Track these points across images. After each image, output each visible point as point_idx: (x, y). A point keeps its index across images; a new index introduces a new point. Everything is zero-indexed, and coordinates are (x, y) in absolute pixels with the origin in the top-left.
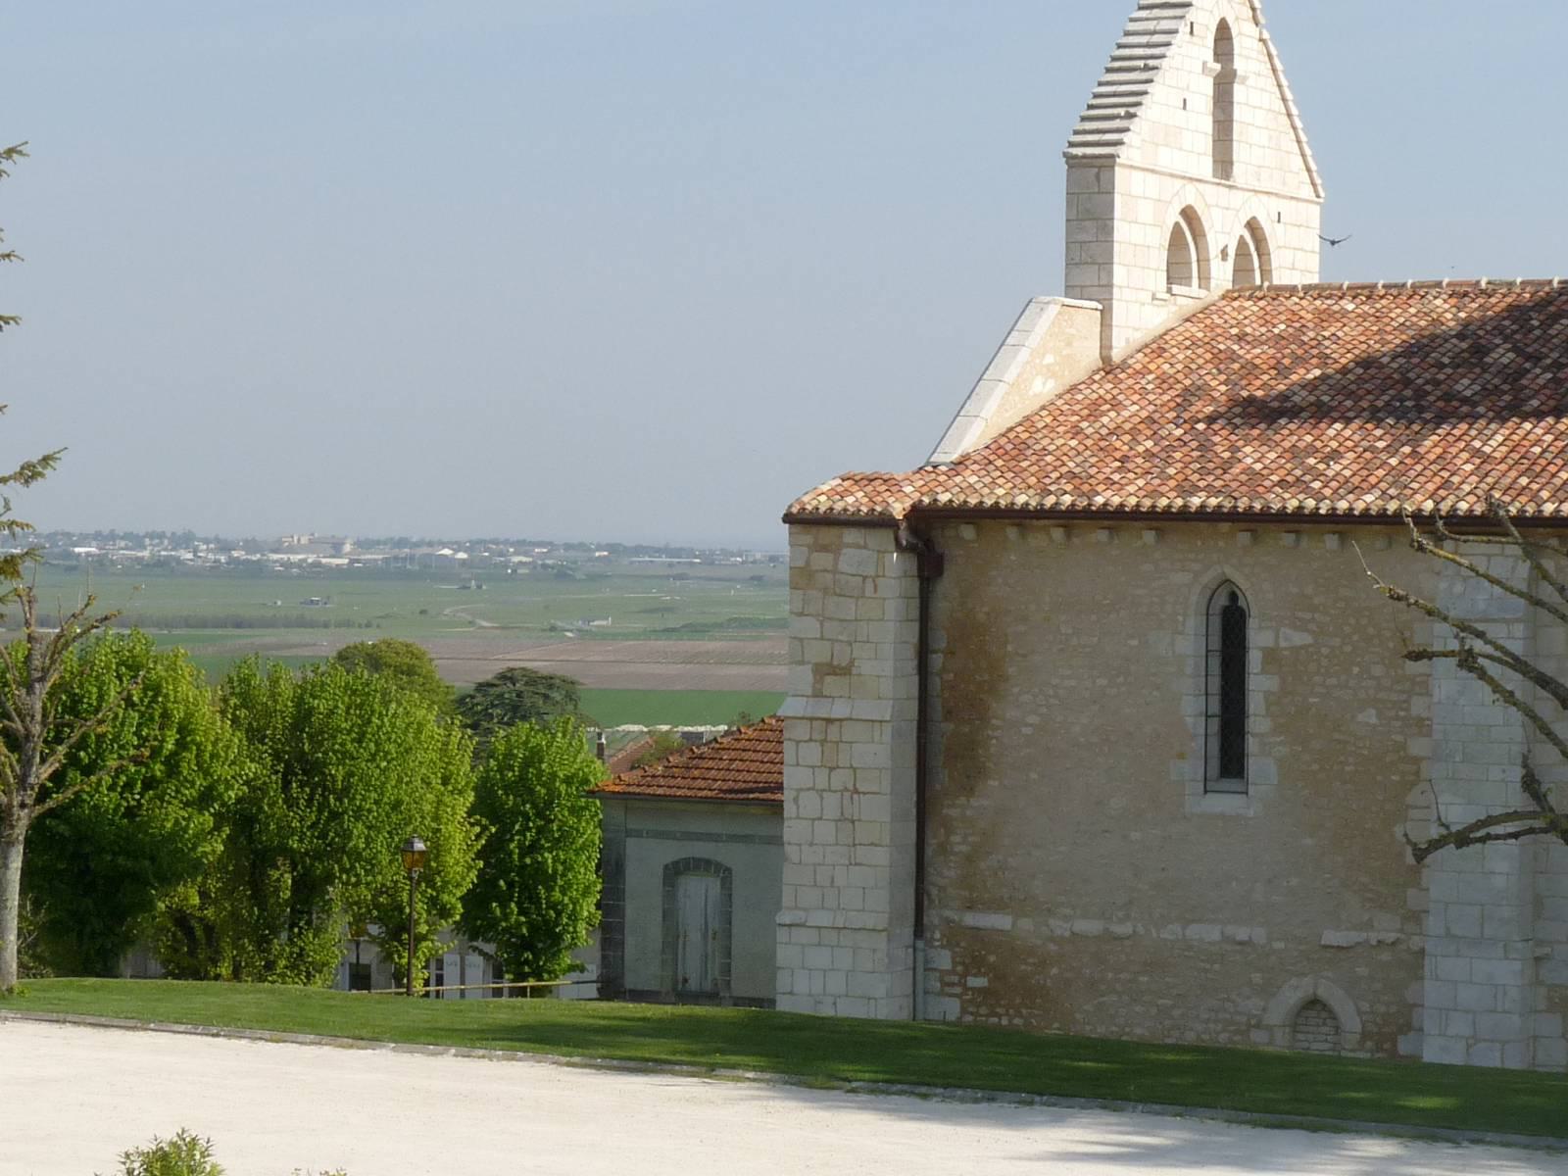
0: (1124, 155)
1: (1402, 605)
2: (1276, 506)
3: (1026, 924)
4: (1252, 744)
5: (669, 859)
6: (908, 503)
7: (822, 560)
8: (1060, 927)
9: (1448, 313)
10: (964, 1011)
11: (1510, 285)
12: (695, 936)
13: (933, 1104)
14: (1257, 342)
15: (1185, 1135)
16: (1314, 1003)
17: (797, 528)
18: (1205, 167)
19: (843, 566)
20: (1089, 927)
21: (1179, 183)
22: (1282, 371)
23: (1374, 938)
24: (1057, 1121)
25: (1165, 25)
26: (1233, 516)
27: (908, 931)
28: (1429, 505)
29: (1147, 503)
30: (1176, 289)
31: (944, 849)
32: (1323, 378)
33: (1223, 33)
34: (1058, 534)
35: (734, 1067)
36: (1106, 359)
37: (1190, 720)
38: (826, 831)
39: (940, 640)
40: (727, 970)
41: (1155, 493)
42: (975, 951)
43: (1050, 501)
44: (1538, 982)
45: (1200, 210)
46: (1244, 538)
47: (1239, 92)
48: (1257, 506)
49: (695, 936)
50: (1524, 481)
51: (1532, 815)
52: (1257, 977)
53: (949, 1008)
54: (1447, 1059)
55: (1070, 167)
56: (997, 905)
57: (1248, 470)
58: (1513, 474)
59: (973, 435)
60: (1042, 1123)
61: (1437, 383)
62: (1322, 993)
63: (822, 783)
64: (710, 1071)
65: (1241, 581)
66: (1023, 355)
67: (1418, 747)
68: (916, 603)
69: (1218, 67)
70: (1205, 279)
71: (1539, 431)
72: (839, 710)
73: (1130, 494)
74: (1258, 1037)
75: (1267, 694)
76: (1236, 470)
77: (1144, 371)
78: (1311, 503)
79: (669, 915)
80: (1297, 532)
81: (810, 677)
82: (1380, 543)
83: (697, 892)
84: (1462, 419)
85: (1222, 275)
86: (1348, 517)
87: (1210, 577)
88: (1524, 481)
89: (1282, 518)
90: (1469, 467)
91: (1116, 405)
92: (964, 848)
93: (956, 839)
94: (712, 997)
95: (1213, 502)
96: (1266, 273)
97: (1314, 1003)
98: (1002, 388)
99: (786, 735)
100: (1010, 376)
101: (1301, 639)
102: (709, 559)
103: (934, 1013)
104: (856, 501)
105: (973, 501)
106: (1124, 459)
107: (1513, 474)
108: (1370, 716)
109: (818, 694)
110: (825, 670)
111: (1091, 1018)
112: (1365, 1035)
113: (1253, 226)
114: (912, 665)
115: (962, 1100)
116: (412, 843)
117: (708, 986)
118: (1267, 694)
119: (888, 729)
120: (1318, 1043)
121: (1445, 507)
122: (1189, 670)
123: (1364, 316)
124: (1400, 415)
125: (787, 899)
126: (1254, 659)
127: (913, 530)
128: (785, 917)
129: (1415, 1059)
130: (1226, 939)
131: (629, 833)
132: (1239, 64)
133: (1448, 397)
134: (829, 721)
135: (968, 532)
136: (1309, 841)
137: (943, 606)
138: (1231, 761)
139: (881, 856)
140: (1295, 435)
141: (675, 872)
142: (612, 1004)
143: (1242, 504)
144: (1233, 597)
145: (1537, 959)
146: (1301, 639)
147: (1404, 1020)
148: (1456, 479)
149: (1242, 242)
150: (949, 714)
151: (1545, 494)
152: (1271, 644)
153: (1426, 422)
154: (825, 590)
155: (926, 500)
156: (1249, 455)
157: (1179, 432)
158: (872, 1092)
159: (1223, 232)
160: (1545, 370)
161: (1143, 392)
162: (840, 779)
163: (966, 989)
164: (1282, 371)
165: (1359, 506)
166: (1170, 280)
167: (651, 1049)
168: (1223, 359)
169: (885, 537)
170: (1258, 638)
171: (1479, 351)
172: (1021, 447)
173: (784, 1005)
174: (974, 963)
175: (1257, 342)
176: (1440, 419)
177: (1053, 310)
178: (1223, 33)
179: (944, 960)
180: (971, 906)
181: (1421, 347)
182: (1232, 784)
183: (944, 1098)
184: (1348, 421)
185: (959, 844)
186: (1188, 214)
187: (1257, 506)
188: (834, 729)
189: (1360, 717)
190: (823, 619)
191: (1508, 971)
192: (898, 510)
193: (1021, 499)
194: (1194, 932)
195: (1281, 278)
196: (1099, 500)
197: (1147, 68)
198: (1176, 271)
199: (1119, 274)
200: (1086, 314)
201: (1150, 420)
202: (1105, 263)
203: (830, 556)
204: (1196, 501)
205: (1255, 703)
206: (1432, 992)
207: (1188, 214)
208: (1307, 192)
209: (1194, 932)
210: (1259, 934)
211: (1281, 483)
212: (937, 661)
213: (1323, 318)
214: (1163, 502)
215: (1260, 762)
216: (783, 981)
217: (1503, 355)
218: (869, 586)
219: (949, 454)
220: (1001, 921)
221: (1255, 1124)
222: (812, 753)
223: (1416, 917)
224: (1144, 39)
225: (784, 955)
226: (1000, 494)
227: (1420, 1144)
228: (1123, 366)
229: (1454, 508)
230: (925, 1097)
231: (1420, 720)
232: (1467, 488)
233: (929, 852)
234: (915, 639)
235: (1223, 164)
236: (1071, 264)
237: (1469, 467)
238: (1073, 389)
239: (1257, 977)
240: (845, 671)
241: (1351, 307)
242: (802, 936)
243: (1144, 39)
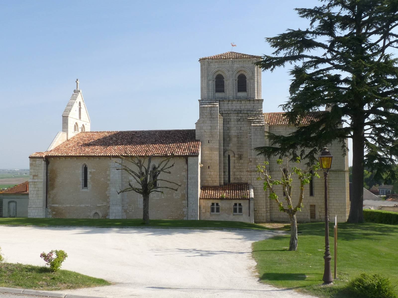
0: (69, 116)
1: (116, 163)
2: (91, 155)
3: (60, 206)
4: (88, 183)
5: (9, 201)
6: (45, 155)
7: (34, 162)
8: (65, 206)
9: (107, 135)
10: (52, 216)
11: (114, 132)
12: (12, 210)
13: (57, 228)
14: (85, 137)
15: (92, 230)
16: (96, 213)
17: (31, 159)
18: (78, 118)
19: (36, 163)
20: (68, 205)
21: (75, 119)
22: (89, 141)
23: (103, 205)
24: (75, 229)
25: (74, 101)
26: (86, 156)
27: (45, 207)
28: (110, 155)
29: (75, 155)
30: (75, 131)
31: (49, 197)
32: (94, 141)
33: (80, 103)
34: (64, 159)
35: (29, 225)
36: (67, 139)
37: (80, 180)
38: (34, 196)
39: (49, 172)
40: (16, 214)
41: (76, 154)
42: (53, 209)
43: (63, 155)
44: (123, 209)
45: (78, 123)
46: (87, 159)
47: (82, 110)
48: (89, 155)
49: (12, 210)
50: (120, 152)
51: (129, 188)
52: (89, 210)
53: (50, 216)
54: (112, 219)
55: (63, 117)
56: (57, 204)
57: (87, 151)
58: (119, 151)
59: (52, 148)
60: (73, 229)
61: (108, 142)
62: (97, 212)
63: (34, 190)
64: (26, 226)
65: (87, 164)
66: (58, 138)
67: (108, 182)
68: (46, 167)
69: (79, 107)
70: (78, 131)
71: (120, 146)
72: (36, 181)
73: (73, 154)
74: (90, 218)
75: (90, 177)
76: (86, 151)
77: (72, 141)
78: (95, 155)
79: (9, 208)
80: (94, 158)
81: (32, 177)
82: (104, 159)
83: (12, 205)
84: (111, 145)
85: (80, 130)
86: (100, 156)
87: (83, 163)
88: (120, 152)
89: (92, 156)
90: (113, 150)
91: (69, 144)
92: (52, 197)
93: (51, 196)
94: (14, 217)
95: (83, 155)
96: (84, 130)
97: (96, 213)
98: (55, 142)
99: (29, 184)
100: (56, 141)
101: (94, 170)
102: (3, 170)
103: (48, 217)
104: (38, 155)
105: (53, 155)
106: (71, 150)
107: (119, 151)
108: (103, 179)
109: (33, 179)
110: (34, 176)
111: (68, 216)
112: (102, 217)
113: (83, 125)
114: (45, 175)
115: (61, 227)
116: (387, 78)
117: (14, 216)
118: (90, 177)
119: (42, 183)
120: (96, 218)
121: (111, 155)
122: (80, 174)
123: (98, 135)
124: (104, 145)
125: (29, 204)
126: (88, 173)
127: (46, 159)
128: (29, 206)
129: (109, 219)
130: (85, 206)
131: (3, 198)
132: (81, 106)
133: (109, 143)
134: (35, 182)
135: (52, 159)
136: (95, 194)
137: (49, 168)
138: (86, 185)
139: (42, 198)
140: (91, 147)
141: (9, 202)
142: (348, 189)
143: (87, 155)
144: (86, 166)
145: (123, 206)
146: (94, 170)
147: (107, 214)
148: (112, 152)
149: (82, 127)
150: (50, 181)
151: (123, 153)
152: (90, 171)
153: (107, 146)
154: (34, 166)
155: (47, 155)
156: (87, 149)
157: (78, 147)
158: (48, 227)
159: (80, 126)
160: (120, 140)
161: (73, 143)
162: (36, 189)
163: (53, 214)
164: (89, 141)
165: (101, 155)
166: (75, 131)
167: (16, 223)
168: (81, 139)
169: (42, 159)
170: (89, 171)
171: (112, 138)
172: (58, 149)
173: (29, 217)
174: (53, 211)
175: (85, 137)
176: (109, 146)
177: (61, 133)
178: (80, 103)
179: (50, 210)
180: (53, 204)
181: (105, 138)
182: (86, 188)
183: (58, 227)
184: (98, 146)
185: (51, 196)
186: (76, 123)
187: (89, 155)
188: (36, 183)
189: (101, 179)
190: (34, 169)
191: (119, 208)
192: (44, 156)
193: (59, 155)
194: (81, 205)
195: (86, 131)
196: (69, 155)
197: (71, 106)
198: (75, 130)
199: (69, 129)
200: (65, 134)
201: (74, 146)
202: (67, 128)
203: (35, 162)
204: (81, 155)
205: (88, 178)
206: (111, 211)
207: (76, 123)
208: (89, 122)
209: (81, 205)
210: (89, 205)
211: (91, 152)
212: (48, 174)
213: (93, 135)
214: (77, 155)
215: (89, 185)
216: (29, 214)
217: (114, 139)
218: (40, 166)
219: (49, 150)
220: (57, 205)
221: (100, 227)
222: (33, 186)
223: (108, 202)
224: (71, 103)
225: (29, 211)
226: (56, 154)
227: (121, 228)
228: (70, 140)
229: (113, 155)
230: (56, 227)
231: (109, 179)
232: (114, 153)
233: (48, 197)
234: (46, 172)
235: (80, 118)
236: (63, 128)
237: (113, 150)
238: (64, 143)
239: (89, 210)
240: (37, 176)
241: (95, 134)
242: (31, 208)
243: (71, 103)
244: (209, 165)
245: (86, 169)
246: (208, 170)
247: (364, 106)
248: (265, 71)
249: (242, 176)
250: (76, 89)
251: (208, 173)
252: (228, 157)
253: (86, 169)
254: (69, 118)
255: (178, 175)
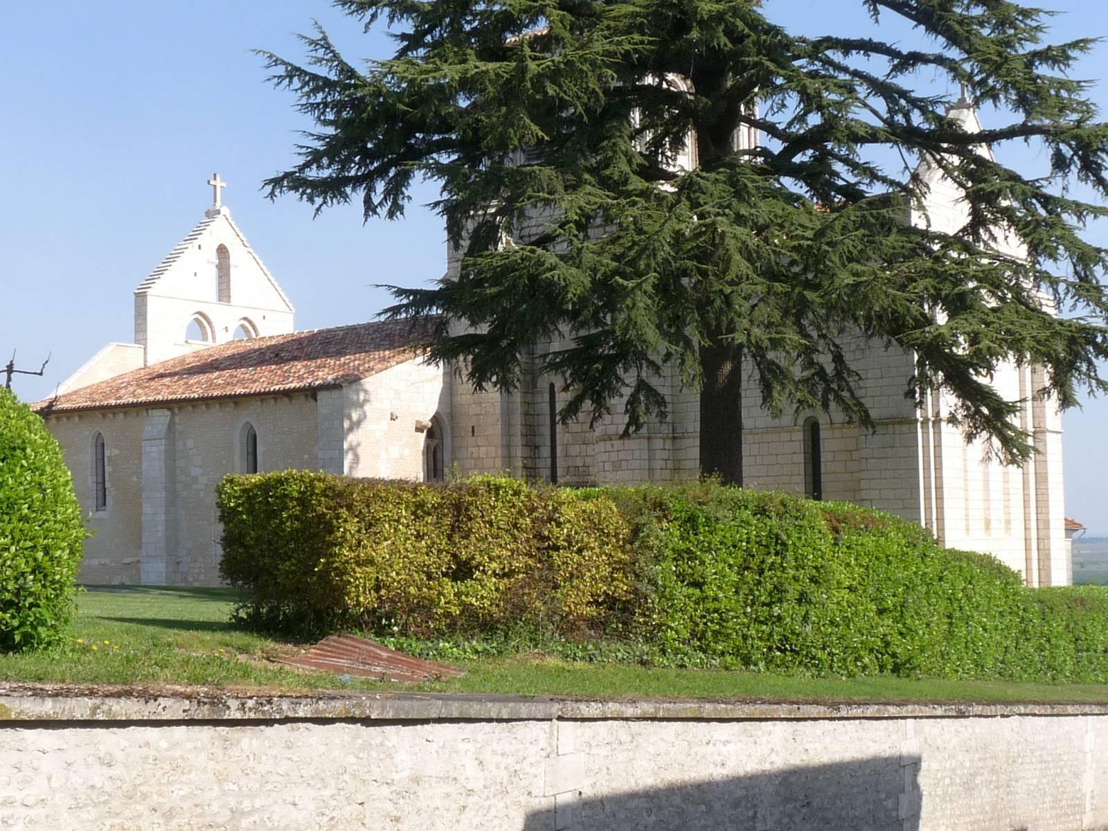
33: (222, 251)
178: (222, 251)
208: (288, 310)
244: (473, 422)
245: (100, 446)
246: (471, 440)
247: (923, 130)
248: (291, 95)
249: (589, 461)
250: (211, 208)
251: (471, 449)
252: (548, 390)
253: (100, 446)
254: (148, 298)
255: (306, 457)
